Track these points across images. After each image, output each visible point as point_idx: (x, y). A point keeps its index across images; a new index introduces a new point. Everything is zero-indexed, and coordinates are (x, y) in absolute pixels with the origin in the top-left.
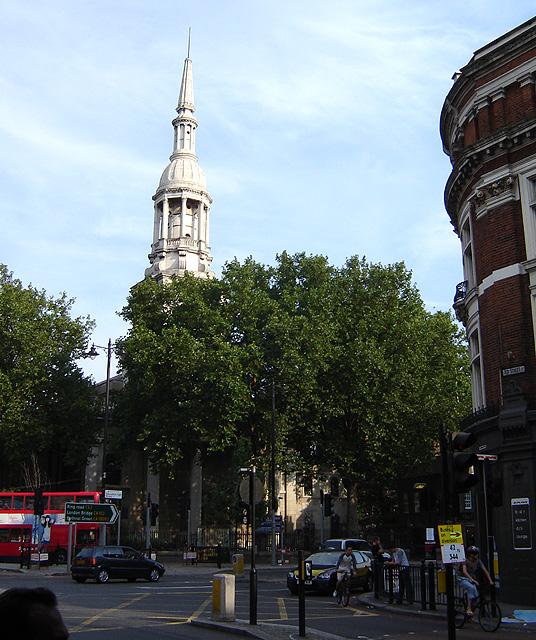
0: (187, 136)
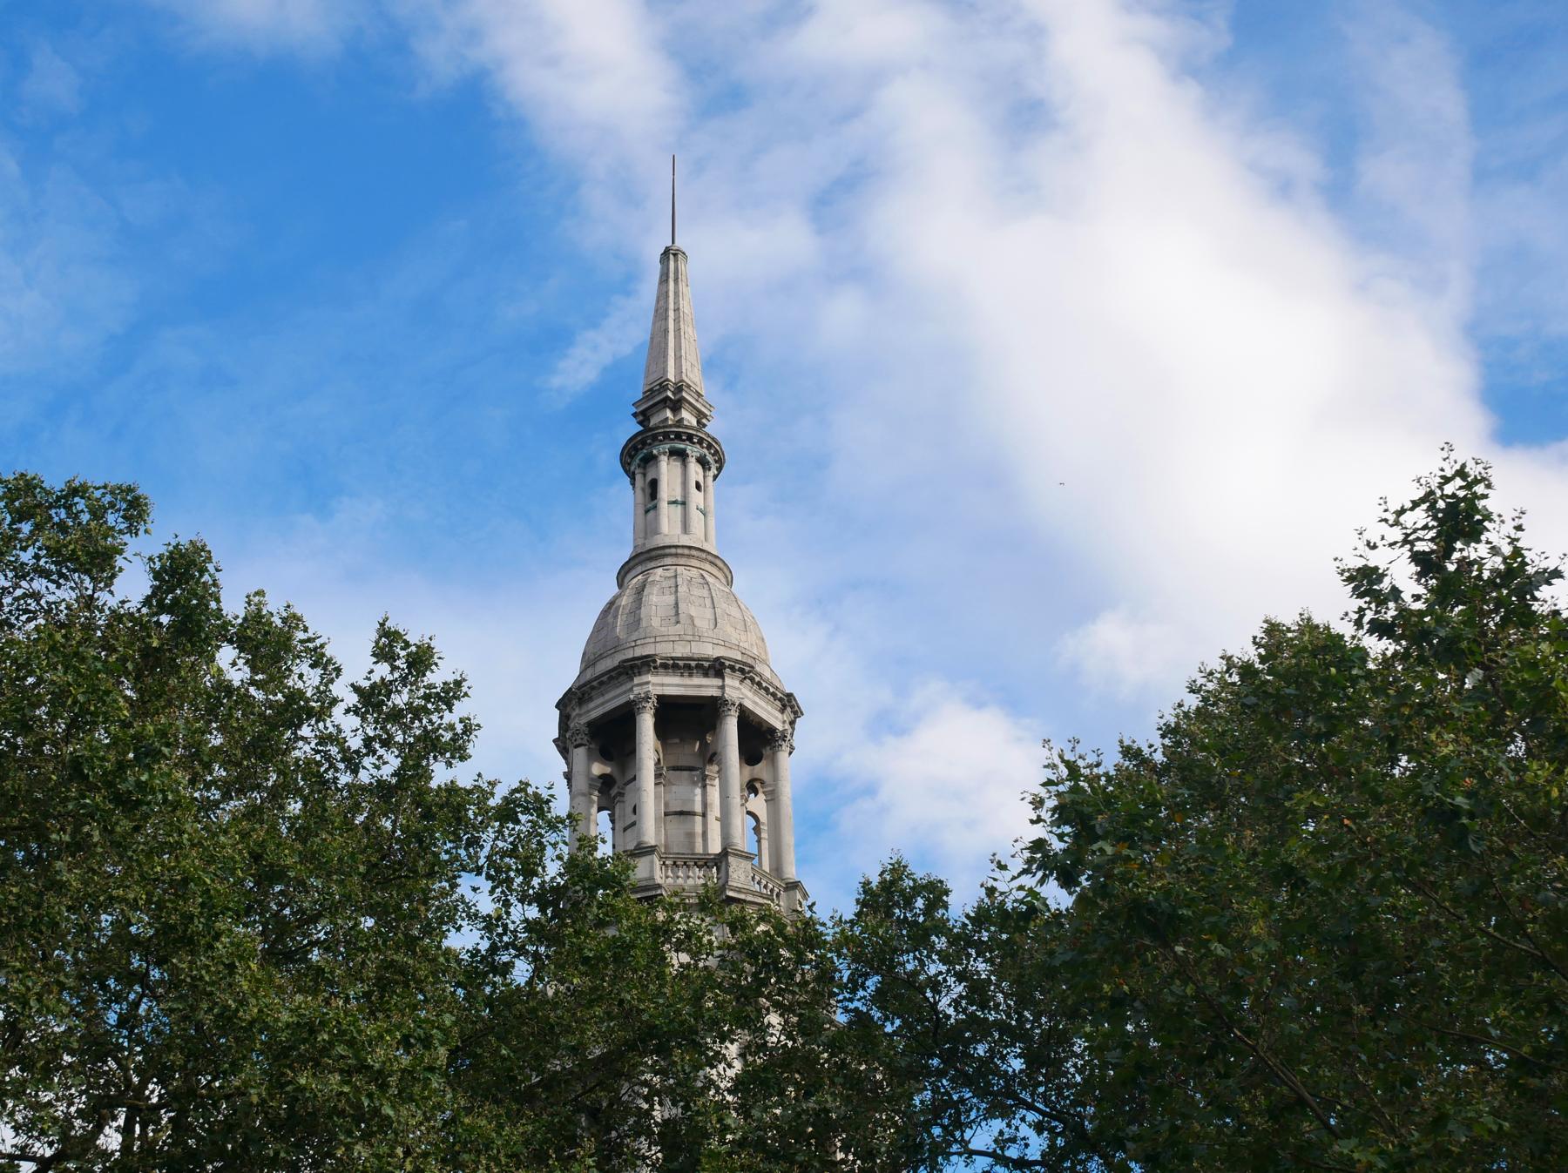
0: (696, 498)
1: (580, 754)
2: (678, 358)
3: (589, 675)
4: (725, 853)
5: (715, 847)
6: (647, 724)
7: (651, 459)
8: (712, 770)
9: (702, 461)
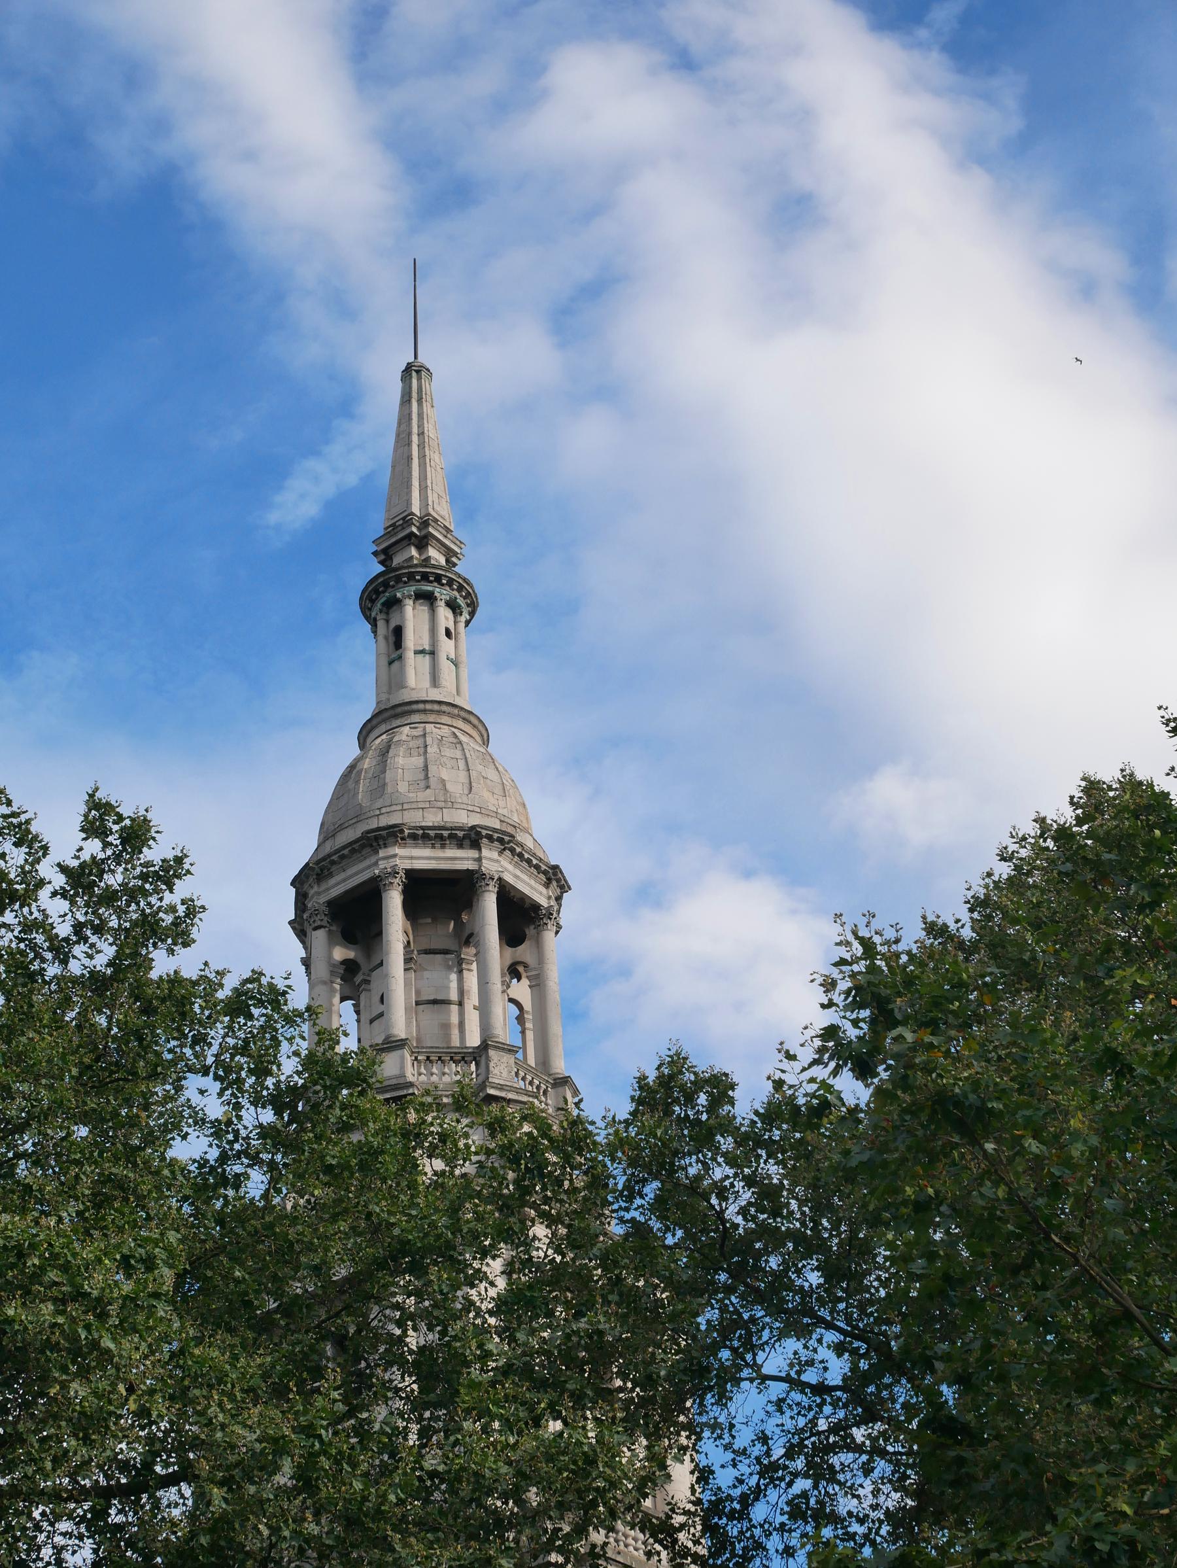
1: (319, 938)
2: (423, 489)
3: (328, 848)
4: (484, 1046)
5: (474, 1040)
6: (394, 902)
7: (394, 604)
8: (468, 952)
9: (452, 606)
